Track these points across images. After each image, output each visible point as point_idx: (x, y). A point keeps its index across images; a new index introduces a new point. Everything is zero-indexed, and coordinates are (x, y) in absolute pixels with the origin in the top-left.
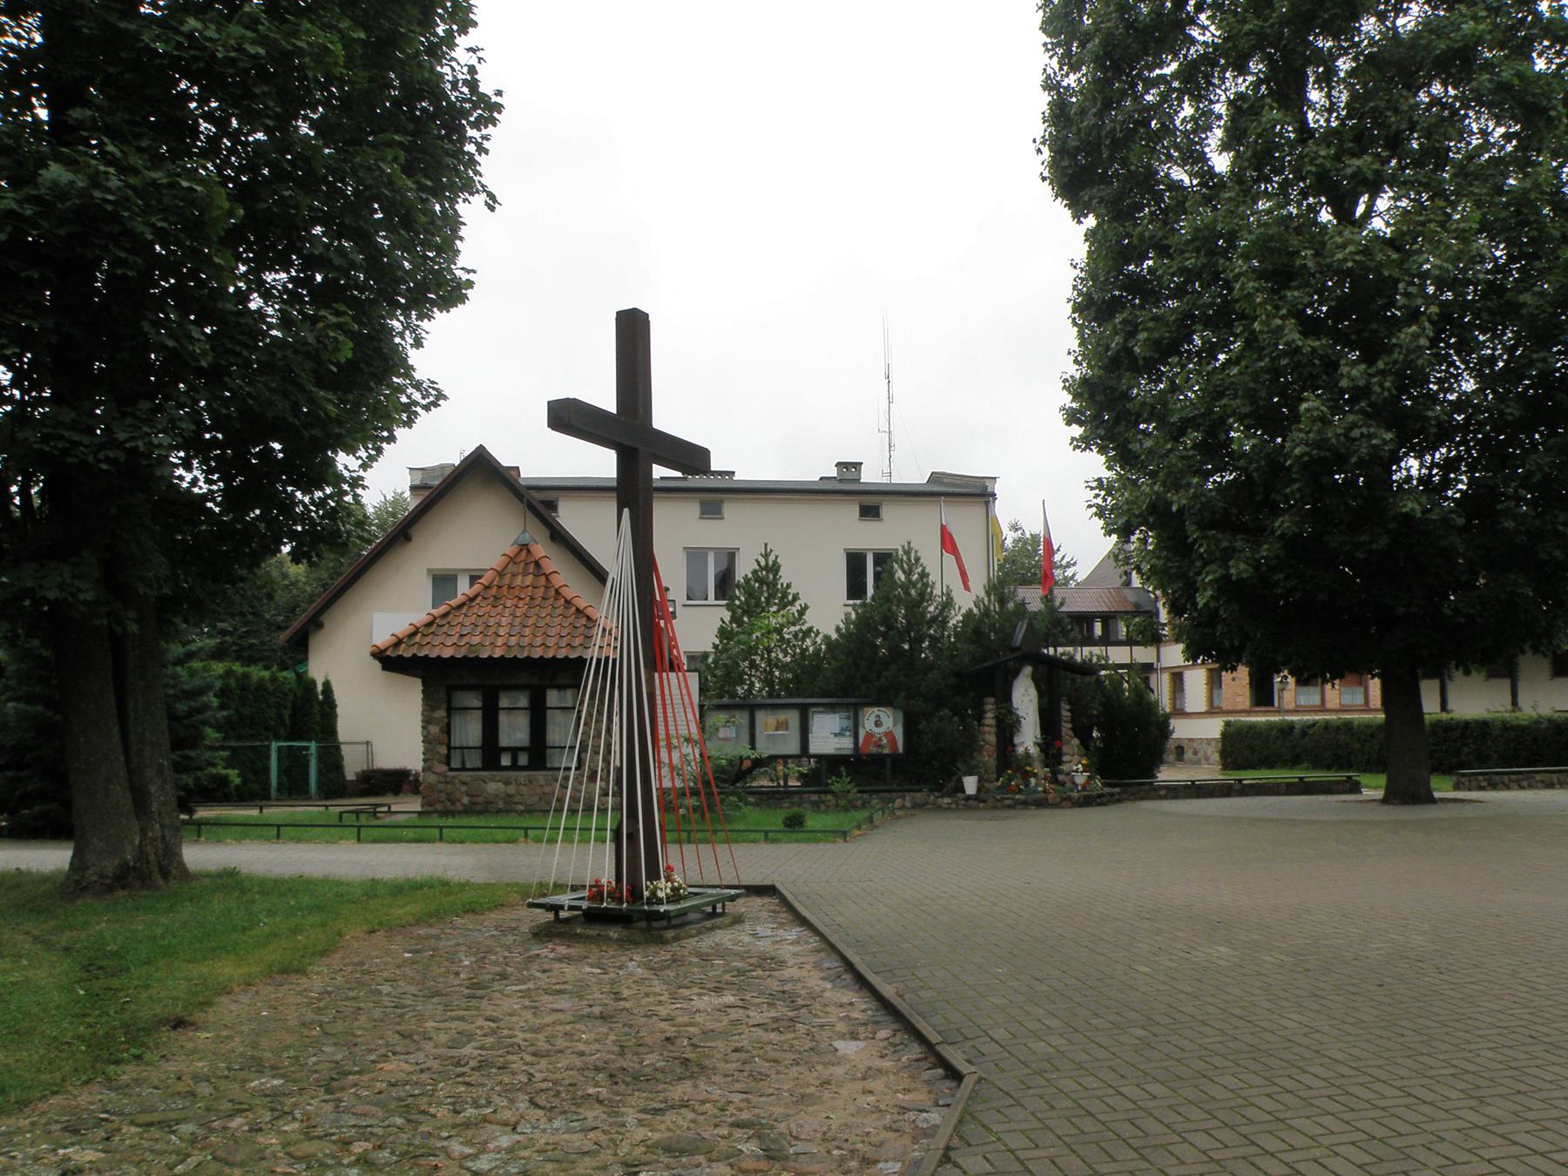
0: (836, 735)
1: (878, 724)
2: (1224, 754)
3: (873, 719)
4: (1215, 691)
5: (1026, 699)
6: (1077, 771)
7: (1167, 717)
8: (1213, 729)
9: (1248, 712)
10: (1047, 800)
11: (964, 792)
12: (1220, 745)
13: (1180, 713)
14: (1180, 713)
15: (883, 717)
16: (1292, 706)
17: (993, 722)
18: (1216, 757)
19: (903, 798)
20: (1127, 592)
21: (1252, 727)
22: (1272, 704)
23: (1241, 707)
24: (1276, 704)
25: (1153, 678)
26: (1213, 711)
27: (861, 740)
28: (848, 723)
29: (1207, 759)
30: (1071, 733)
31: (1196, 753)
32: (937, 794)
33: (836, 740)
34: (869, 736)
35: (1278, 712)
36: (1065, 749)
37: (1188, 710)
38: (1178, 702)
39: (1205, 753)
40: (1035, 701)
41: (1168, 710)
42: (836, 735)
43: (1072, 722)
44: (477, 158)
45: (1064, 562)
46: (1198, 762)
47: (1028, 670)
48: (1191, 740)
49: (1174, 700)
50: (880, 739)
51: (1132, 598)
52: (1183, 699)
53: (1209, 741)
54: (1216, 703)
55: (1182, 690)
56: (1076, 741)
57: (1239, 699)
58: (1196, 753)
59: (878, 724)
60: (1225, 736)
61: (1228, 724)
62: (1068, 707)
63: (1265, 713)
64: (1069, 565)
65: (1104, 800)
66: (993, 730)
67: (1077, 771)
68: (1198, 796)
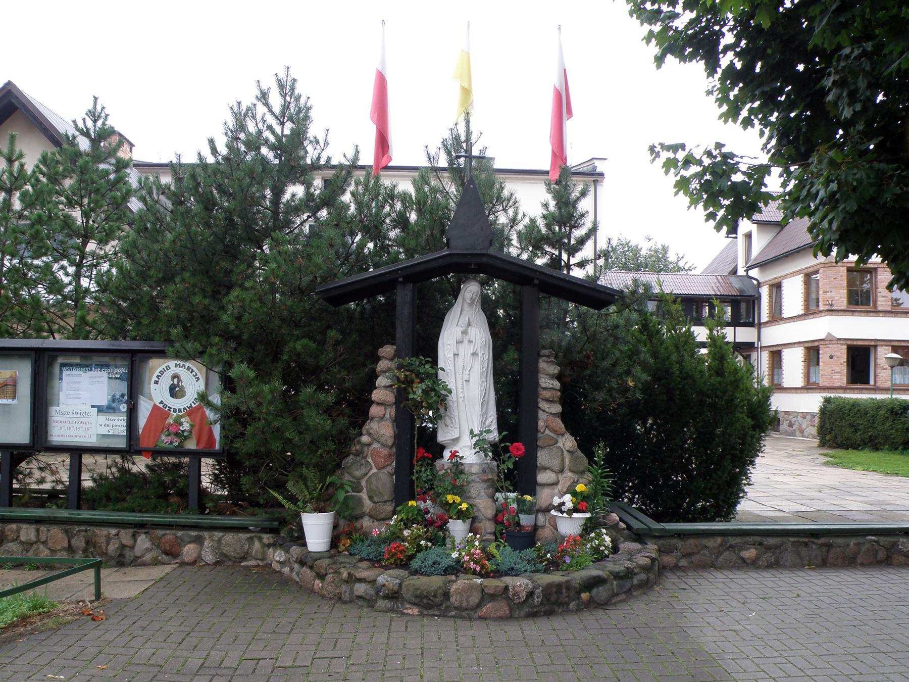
0: (101, 410)
1: (176, 391)
2: (823, 431)
3: (166, 381)
4: (812, 369)
5: (466, 350)
6: (559, 508)
7: (765, 395)
8: (813, 403)
9: (844, 389)
10: (446, 595)
11: (305, 545)
12: (817, 420)
13: (780, 388)
14: (780, 388)
15: (184, 374)
16: (888, 384)
17: (390, 397)
18: (814, 431)
19: (199, 540)
20: (732, 279)
21: (855, 404)
22: (868, 382)
23: (837, 384)
24: (872, 382)
25: (754, 355)
26: (809, 386)
27: (142, 422)
28: (122, 388)
29: (802, 432)
30: (559, 424)
31: (791, 425)
32: (267, 538)
33: (102, 419)
34: (159, 413)
35: (876, 389)
36: (543, 457)
37: (785, 385)
38: (776, 377)
39: (800, 425)
40: (486, 356)
41: (766, 383)
42: (101, 410)
43: (563, 401)
44: (602, 245)
45: (686, 268)
46: (793, 434)
47: (471, 290)
48: (787, 413)
49: (772, 375)
50: (178, 423)
51: (736, 284)
52: (780, 374)
53: (804, 415)
54: (813, 380)
55: (781, 367)
56: (568, 442)
57: (837, 376)
58: (791, 425)
59: (176, 391)
60: (824, 412)
61: (827, 401)
62: (555, 369)
63: (861, 390)
64: (690, 269)
65: (601, 592)
66: (391, 412)
67: (559, 508)
68: (823, 564)
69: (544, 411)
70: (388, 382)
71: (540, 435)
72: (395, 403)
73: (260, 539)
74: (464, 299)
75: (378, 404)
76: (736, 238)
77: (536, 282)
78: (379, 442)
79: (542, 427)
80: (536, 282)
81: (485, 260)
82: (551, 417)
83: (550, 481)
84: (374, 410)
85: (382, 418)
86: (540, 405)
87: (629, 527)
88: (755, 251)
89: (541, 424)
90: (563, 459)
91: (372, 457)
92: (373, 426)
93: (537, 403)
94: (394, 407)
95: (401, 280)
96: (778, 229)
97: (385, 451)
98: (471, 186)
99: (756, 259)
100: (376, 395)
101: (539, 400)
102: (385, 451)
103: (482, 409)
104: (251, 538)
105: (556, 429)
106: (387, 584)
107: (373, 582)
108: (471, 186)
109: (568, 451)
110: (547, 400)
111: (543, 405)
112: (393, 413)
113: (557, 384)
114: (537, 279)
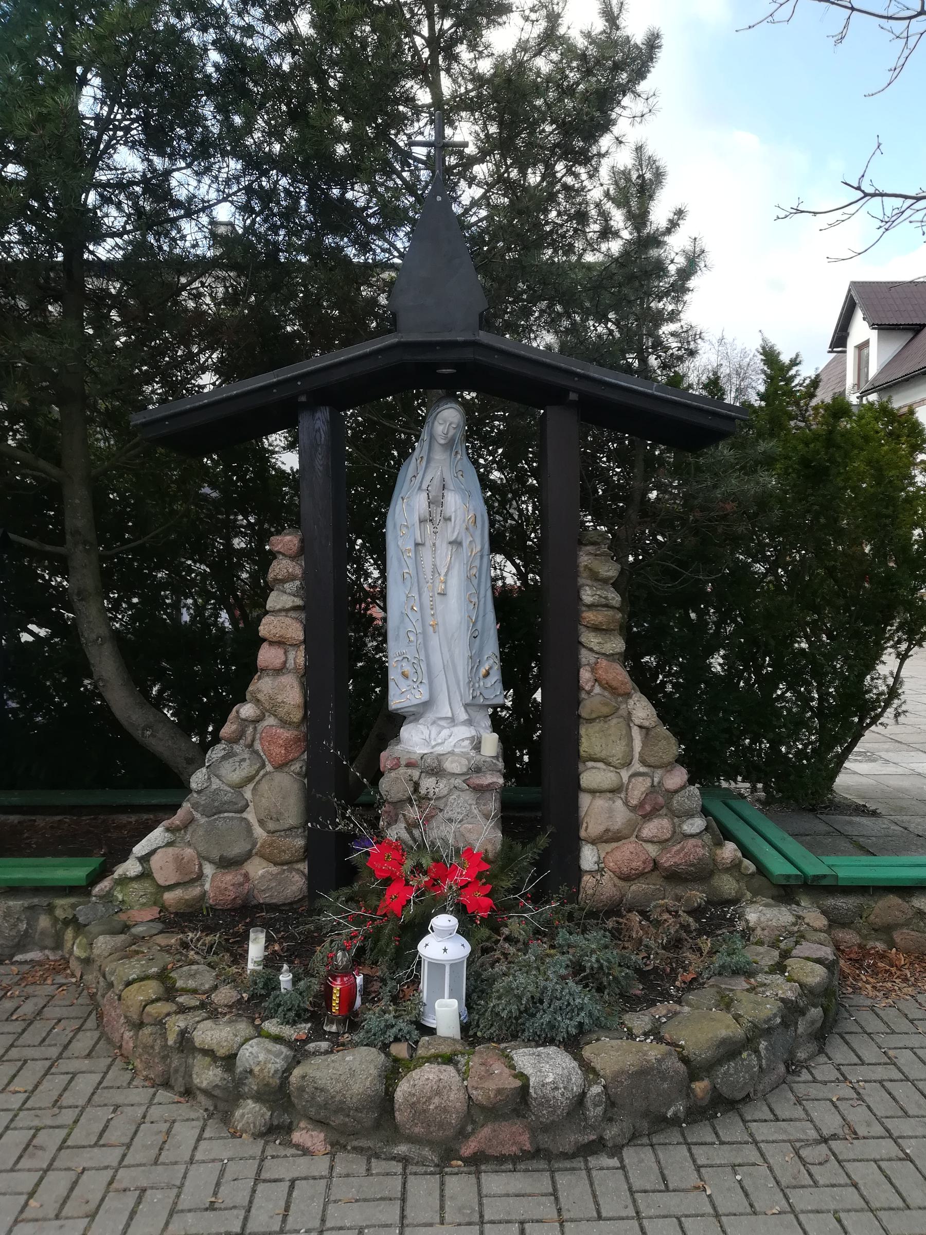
17: (294, 630)
30: (619, 674)
62: (610, 570)
66: (298, 658)
69: (591, 650)
70: (288, 601)
71: (583, 695)
72: (305, 641)
73: (50, 909)
74: (432, 437)
75: (272, 643)
76: (845, 352)
77: (573, 396)
78: (275, 716)
79: (588, 681)
80: (573, 396)
81: (468, 355)
82: (604, 663)
83: (606, 785)
84: (267, 656)
85: (279, 671)
86: (583, 639)
87: (762, 870)
88: (873, 370)
89: (585, 675)
90: (631, 739)
91: (261, 744)
92: (262, 686)
93: (577, 635)
94: (302, 647)
95: (303, 399)
96: (910, 335)
97: (286, 734)
98: (439, 198)
99: (876, 378)
100: (268, 626)
101: (583, 629)
102: (286, 734)
103: (471, 645)
104: (32, 908)
105: (614, 684)
106: (256, 1069)
107: (229, 1060)
108: (439, 198)
109: (640, 727)
110: (596, 629)
111: (590, 639)
112: (301, 660)
113: (615, 598)
114: (575, 391)
